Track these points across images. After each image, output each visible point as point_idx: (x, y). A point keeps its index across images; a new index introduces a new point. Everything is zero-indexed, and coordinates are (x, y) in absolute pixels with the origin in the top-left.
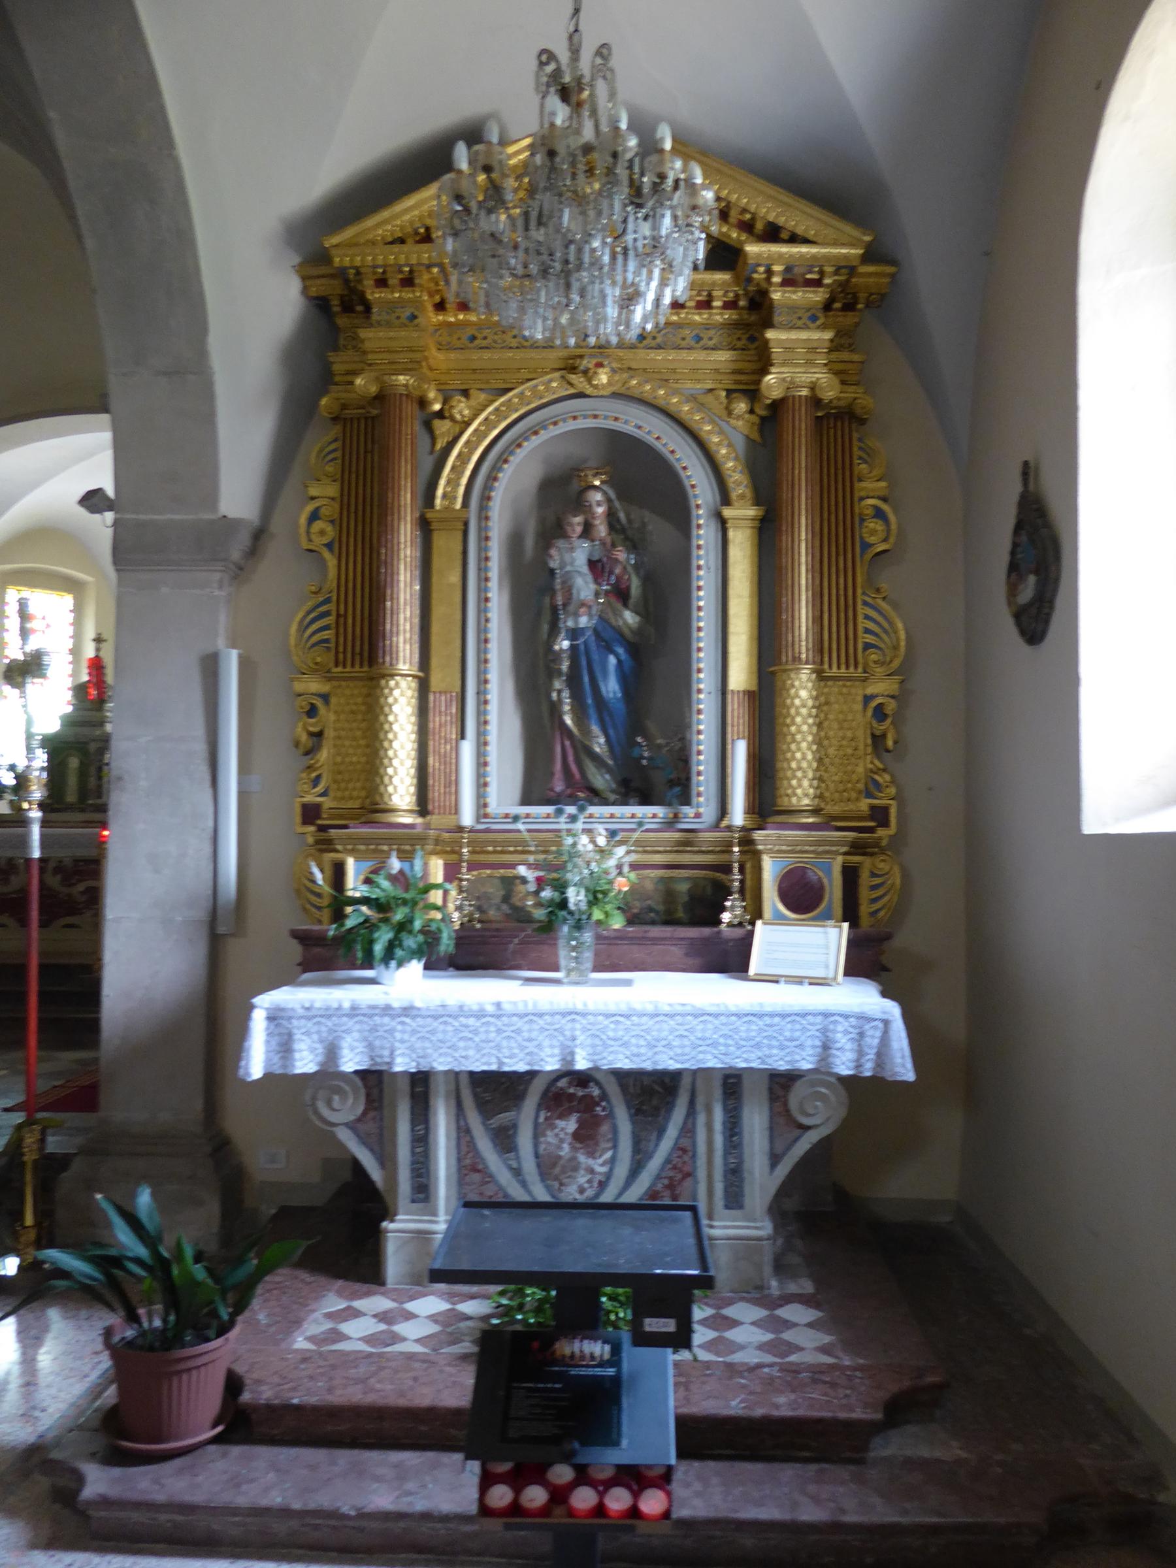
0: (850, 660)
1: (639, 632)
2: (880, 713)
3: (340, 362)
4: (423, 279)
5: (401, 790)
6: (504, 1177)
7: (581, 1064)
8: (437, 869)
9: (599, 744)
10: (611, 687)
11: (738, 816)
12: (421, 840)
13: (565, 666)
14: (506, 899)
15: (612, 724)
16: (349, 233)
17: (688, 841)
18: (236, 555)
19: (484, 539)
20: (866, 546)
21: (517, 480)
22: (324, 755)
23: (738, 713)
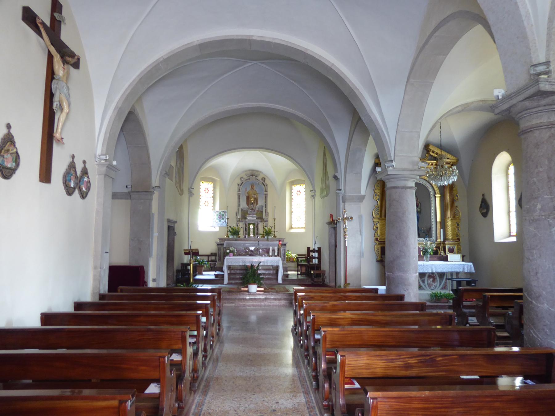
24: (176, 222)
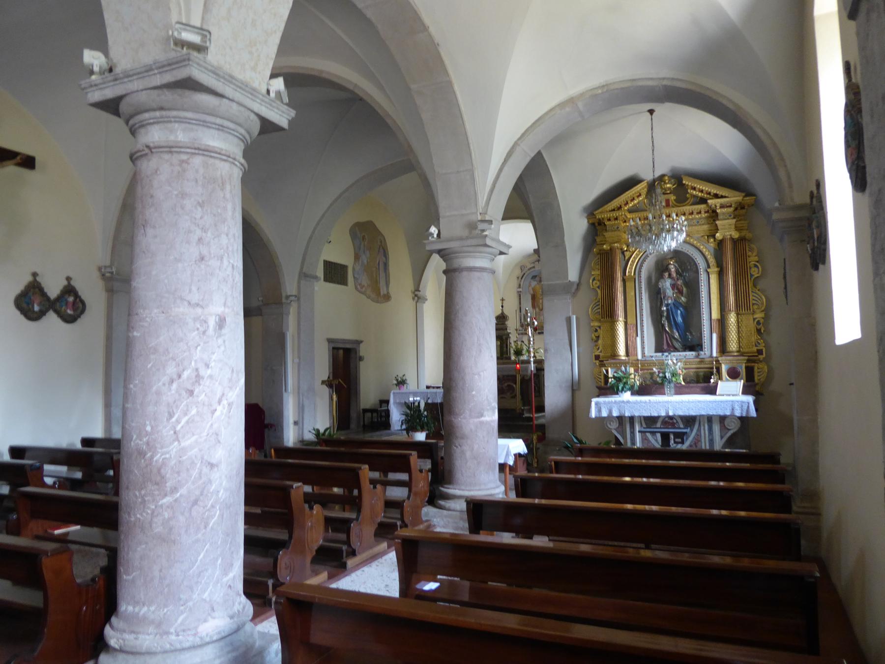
0: (748, 308)
1: (687, 303)
2: (758, 323)
3: (598, 239)
4: (621, 218)
5: (621, 351)
6: (653, 441)
7: (671, 414)
8: (632, 370)
9: (677, 335)
10: (679, 319)
11: (715, 354)
12: (628, 363)
13: (665, 314)
14: (652, 378)
15: (678, 328)
16: (600, 210)
17: (702, 361)
18: (573, 290)
19: (640, 282)
20: (752, 276)
21: (649, 264)
22: (600, 342)
23: (715, 325)
24: (362, 342)
